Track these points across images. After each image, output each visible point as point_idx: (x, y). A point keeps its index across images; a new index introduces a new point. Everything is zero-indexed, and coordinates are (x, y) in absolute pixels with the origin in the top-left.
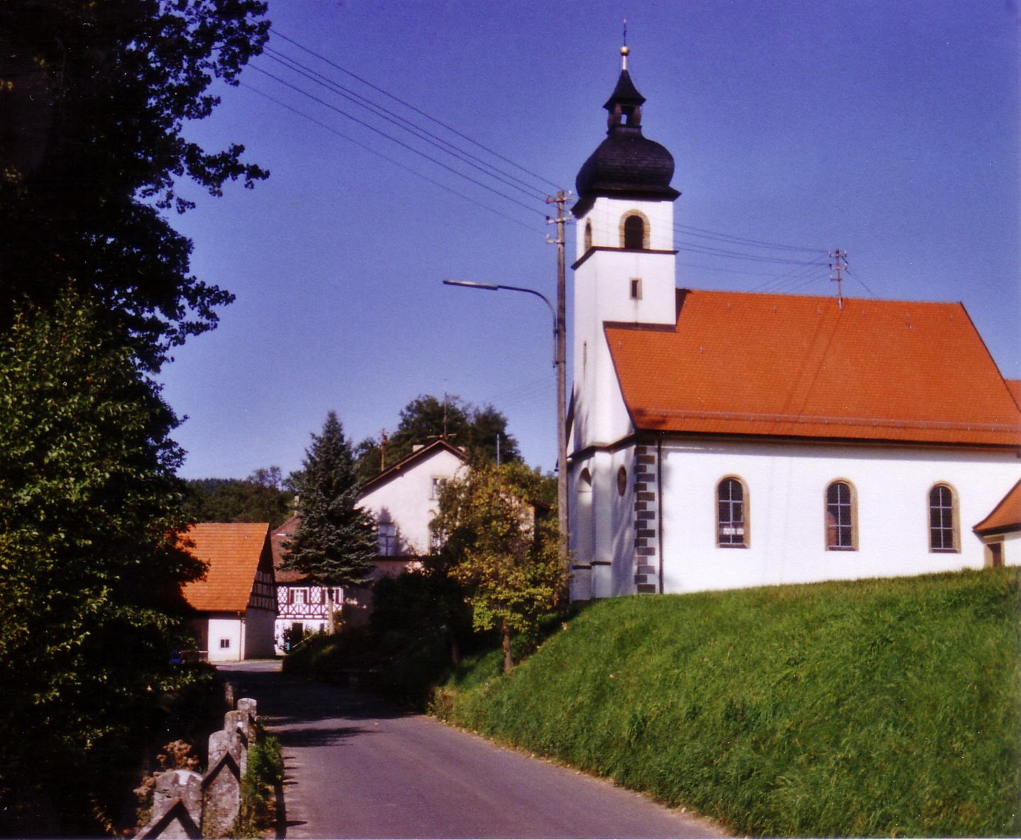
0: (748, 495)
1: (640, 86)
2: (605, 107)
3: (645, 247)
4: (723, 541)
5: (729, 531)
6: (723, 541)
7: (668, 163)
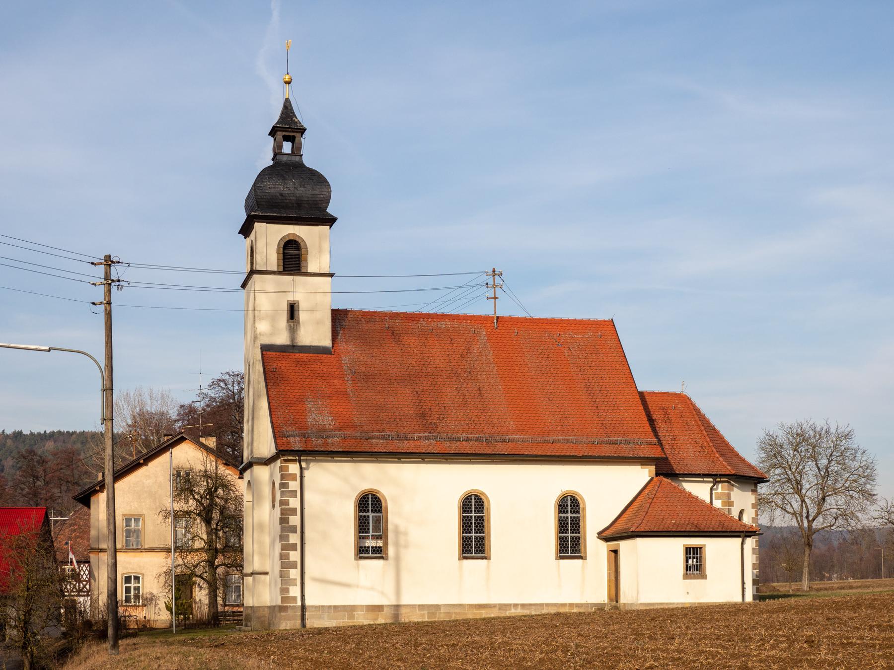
0: (584, 509)
1: (302, 116)
2: (269, 134)
3: (303, 270)
4: (362, 552)
5: (370, 543)
6: (362, 552)
7: (291, 235)
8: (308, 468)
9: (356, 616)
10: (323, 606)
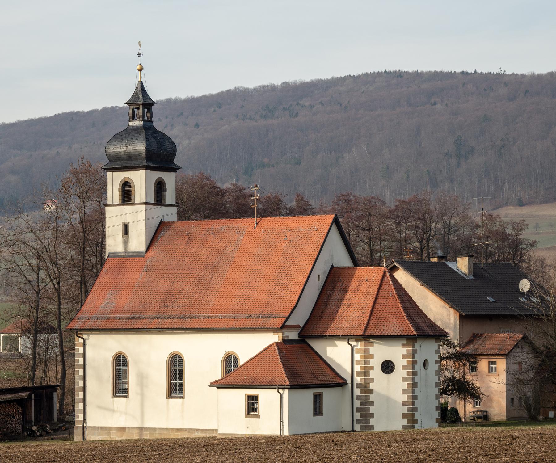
8: (88, 339)
9: (112, 433)
10: (95, 427)
